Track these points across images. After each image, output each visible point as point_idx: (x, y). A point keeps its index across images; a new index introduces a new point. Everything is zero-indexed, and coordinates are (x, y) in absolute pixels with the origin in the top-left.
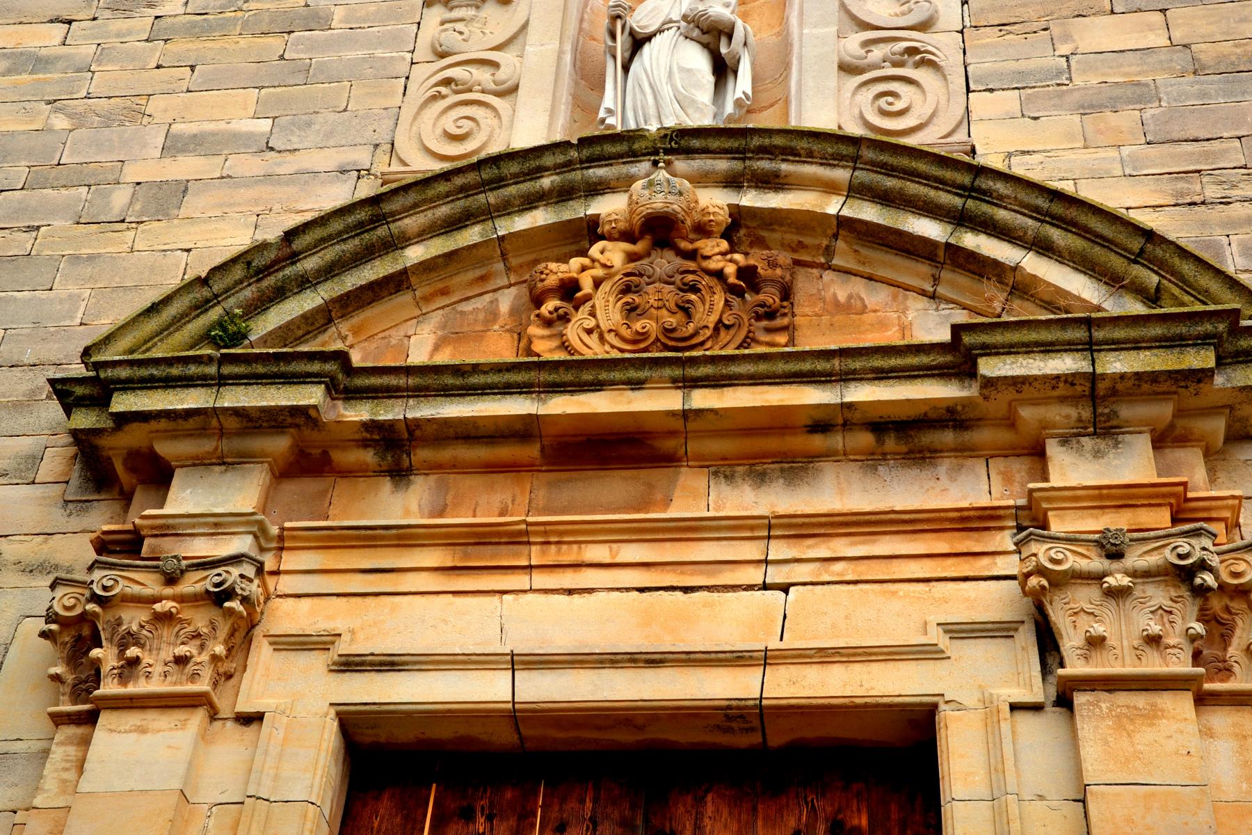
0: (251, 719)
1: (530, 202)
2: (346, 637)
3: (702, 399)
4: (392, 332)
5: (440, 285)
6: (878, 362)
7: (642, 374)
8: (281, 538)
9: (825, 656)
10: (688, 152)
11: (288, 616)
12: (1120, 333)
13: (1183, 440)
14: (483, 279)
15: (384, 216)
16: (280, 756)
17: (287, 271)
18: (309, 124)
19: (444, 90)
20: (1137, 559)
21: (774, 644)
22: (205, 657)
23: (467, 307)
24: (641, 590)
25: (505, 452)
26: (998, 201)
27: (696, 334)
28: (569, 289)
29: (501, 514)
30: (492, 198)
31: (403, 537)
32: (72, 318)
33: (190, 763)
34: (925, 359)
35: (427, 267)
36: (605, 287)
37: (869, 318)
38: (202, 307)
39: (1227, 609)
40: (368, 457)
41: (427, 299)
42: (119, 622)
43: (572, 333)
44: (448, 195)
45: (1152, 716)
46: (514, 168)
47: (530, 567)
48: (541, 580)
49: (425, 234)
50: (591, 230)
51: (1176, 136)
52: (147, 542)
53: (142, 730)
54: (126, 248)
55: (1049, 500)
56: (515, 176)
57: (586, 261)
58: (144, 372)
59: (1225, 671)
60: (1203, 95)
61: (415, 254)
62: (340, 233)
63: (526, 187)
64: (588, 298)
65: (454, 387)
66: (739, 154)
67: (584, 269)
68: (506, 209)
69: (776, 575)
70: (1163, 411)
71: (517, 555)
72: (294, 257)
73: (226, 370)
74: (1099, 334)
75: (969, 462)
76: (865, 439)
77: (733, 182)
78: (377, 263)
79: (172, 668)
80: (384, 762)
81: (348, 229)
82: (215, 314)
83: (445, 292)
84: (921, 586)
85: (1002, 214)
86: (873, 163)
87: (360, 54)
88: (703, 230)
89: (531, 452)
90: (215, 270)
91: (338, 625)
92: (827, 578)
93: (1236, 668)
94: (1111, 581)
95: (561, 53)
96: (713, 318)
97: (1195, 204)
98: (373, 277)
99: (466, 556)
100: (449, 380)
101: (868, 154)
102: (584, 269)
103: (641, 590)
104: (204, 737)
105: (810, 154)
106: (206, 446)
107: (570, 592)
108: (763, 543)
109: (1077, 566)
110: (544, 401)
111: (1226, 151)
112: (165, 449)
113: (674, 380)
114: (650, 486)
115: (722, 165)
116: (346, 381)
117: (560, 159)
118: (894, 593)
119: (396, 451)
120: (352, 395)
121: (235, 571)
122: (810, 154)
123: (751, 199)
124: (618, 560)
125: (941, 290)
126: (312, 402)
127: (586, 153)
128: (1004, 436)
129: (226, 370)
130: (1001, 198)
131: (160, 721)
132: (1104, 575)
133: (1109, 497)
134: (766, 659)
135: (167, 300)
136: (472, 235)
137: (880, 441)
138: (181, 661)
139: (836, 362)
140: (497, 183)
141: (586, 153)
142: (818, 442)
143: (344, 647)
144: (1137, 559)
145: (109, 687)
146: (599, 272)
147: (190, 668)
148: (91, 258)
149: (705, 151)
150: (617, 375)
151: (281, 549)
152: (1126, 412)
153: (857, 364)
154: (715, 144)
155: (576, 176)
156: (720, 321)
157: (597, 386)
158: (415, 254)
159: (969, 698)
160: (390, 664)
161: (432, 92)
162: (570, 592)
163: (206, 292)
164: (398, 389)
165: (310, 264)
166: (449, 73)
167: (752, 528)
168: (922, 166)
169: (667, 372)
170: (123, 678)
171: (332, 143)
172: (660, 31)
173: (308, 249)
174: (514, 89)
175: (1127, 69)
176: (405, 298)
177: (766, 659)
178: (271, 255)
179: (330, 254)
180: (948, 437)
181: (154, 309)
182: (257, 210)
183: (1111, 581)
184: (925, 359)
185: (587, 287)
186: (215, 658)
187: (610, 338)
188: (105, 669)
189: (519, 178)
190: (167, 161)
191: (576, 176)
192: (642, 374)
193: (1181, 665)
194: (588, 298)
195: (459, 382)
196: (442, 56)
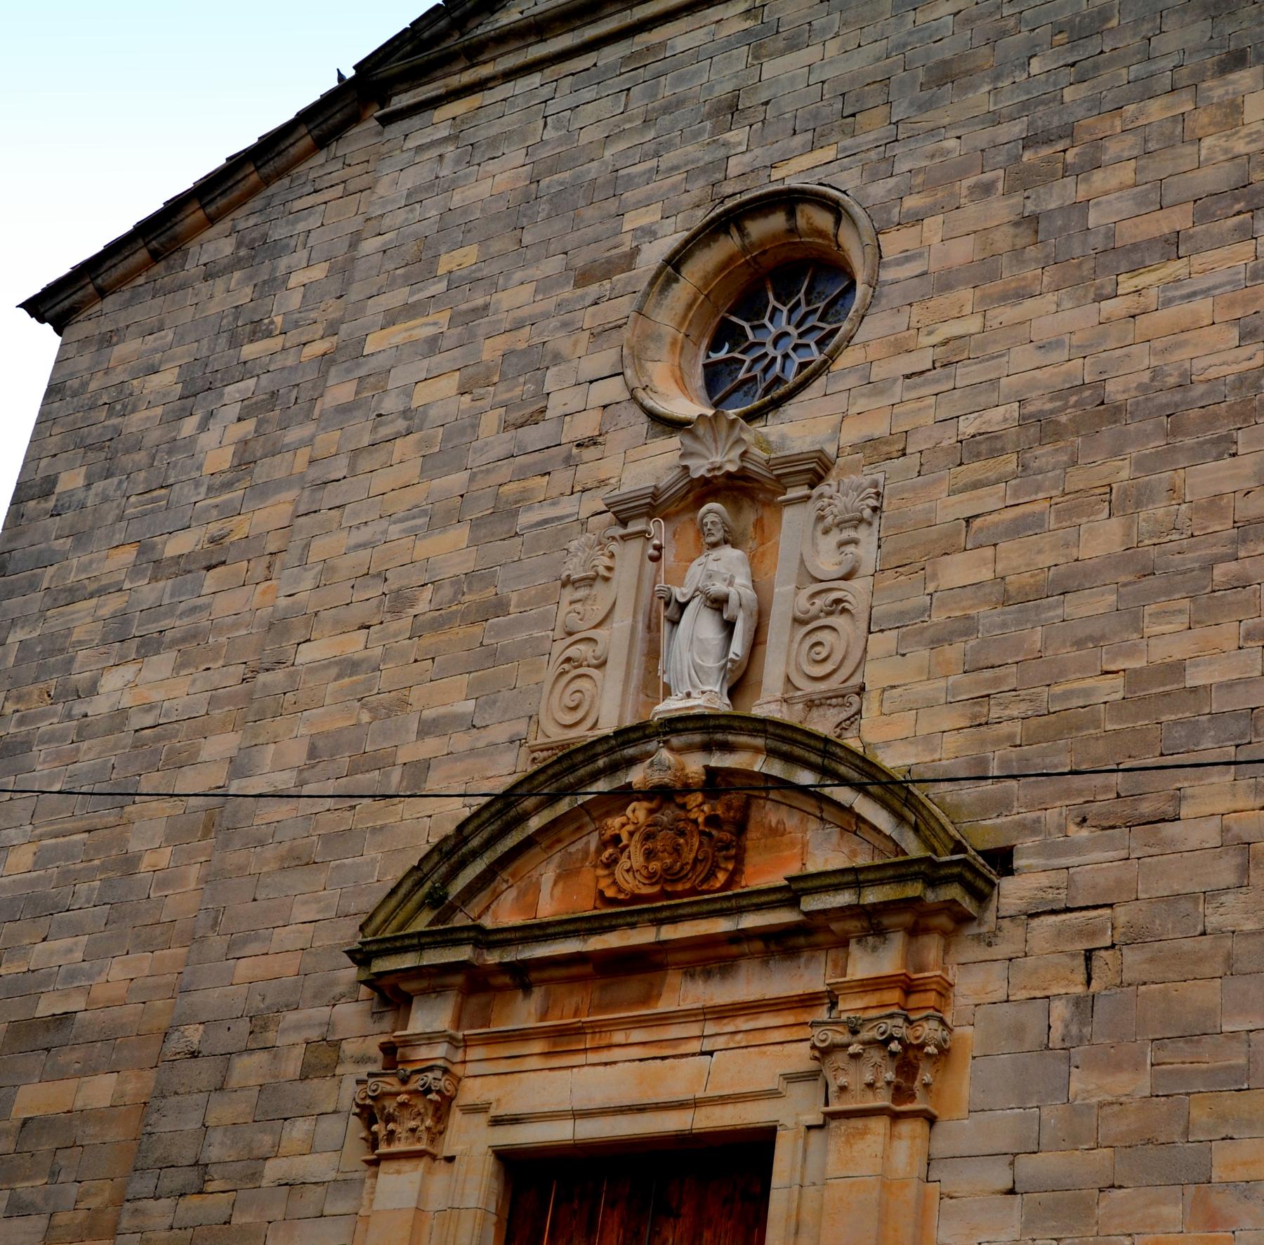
0: (450, 1159)
1: (595, 777)
2: (494, 1105)
3: (669, 933)
4: (533, 872)
5: (555, 838)
6: (755, 900)
7: (634, 919)
8: (464, 1040)
9: (723, 1100)
10: (678, 732)
11: (473, 1091)
12: (871, 876)
13: (927, 931)
14: (580, 828)
15: (512, 803)
16: (464, 1181)
17: (464, 850)
18: (495, 702)
19: (566, 666)
20: (865, 1035)
21: (700, 1094)
22: (422, 1128)
23: (572, 849)
24: (641, 1060)
25: (574, 971)
26: (840, 760)
27: (682, 868)
28: (616, 839)
29: (575, 1016)
30: (570, 779)
31: (523, 1036)
32: (373, 877)
33: (420, 1191)
34: (773, 897)
35: (543, 830)
36: (636, 837)
37: (786, 838)
38: (419, 884)
39: (916, 1057)
40: (506, 980)
41: (550, 847)
42: (384, 1108)
43: (619, 871)
44: (546, 781)
45: (864, 1133)
46: (580, 757)
47: (586, 1050)
48: (593, 1057)
49: (538, 809)
50: (626, 794)
51: (981, 664)
52: (399, 1050)
53: (398, 1172)
54: (398, 818)
55: (838, 989)
56: (582, 762)
57: (623, 819)
58: (384, 946)
59: (912, 1097)
60: (1004, 625)
61: (535, 823)
62: (489, 819)
63: (589, 768)
64: (627, 846)
65: (540, 936)
66: (705, 729)
67: (623, 825)
68: (582, 782)
69: (707, 1048)
70: (907, 918)
71: (579, 1042)
72: (465, 841)
73: (423, 940)
74: (861, 877)
75: (817, 954)
76: (758, 945)
77: (707, 748)
78: (514, 833)
79: (409, 1134)
80: (523, 1172)
81: (492, 816)
82: (428, 885)
83: (559, 841)
84: (779, 1047)
85: (843, 769)
86: (773, 734)
87: (524, 635)
88: (687, 789)
89: (588, 969)
90: (421, 861)
91: (490, 1096)
92: (732, 1045)
93: (918, 1094)
94: (851, 1050)
95: (633, 629)
96: (692, 856)
97: (980, 725)
98: (511, 845)
99: (555, 1045)
100: (537, 933)
101: (771, 729)
102: (623, 825)
103: (641, 1060)
104: (428, 1172)
105: (742, 729)
106: (424, 984)
107: (606, 1064)
108: (701, 1024)
109: (835, 1041)
110: (585, 941)
111: (1007, 676)
112: (405, 987)
113: (651, 921)
114: (651, 985)
115: (697, 738)
116: (483, 938)
117: (606, 747)
118: (765, 1053)
119: (522, 977)
120: (492, 946)
121: (430, 1075)
122: (742, 729)
123: (719, 761)
124: (630, 1041)
125: (825, 816)
126: (465, 958)
127: (620, 740)
128: (830, 938)
129: (423, 940)
130: (840, 758)
131: (406, 1166)
132: (848, 1045)
133: (867, 985)
134: (695, 1104)
135: (399, 885)
136: (563, 806)
137: (767, 946)
138: (413, 1130)
139: (734, 902)
140: (573, 768)
141: (620, 740)
142: (734, 950)
143: (494, 1112)
144: (865, 1035)
145: (383, 1149)
146: (630, 827)
147: (418, 1134)
148: (382, 828)
149: (686, 730)
150: (621, 921)
151: (466, 1046)
152: (886, 921)
153: (744, 902)
154: (691, 725)
155: (617, 756)
156: (696, 857)
157: (612, 929)
158: (535, 823)
159: (789, 1123)
160: (515, 1120)
161: (560, 670)
162: (606, 1064)
163: (420, 874)
164: (511, 940)
165: (475, 842)
166: (571, 652)
167: (695, 1015)
168: (799, 737)
169: (646, 917)
170: (389, 1144)
171: (506, 718)
172: (693, 598)
173: (473, 832)
174: (604, 663)
175: (964, 604)
176: (537, 849)
177: (695, 1104)
178: (452, 842)
179: (485, 834)
180: (802, 941)
181: (393, 892)
182: (466, 779)
183: (851, 1050)
184: (773, 897)
185: (625, 836)
186: (428, 1129)
187: (638, 875)
188: (380, 1136)
189: (586, 762)
190: (419, 742)
191: (617, 756)
192: (634, 919)
193: (882, 1099)
194: (627, 846)
195: (541, 933)
196: (570, 634)
